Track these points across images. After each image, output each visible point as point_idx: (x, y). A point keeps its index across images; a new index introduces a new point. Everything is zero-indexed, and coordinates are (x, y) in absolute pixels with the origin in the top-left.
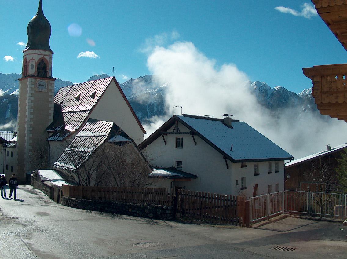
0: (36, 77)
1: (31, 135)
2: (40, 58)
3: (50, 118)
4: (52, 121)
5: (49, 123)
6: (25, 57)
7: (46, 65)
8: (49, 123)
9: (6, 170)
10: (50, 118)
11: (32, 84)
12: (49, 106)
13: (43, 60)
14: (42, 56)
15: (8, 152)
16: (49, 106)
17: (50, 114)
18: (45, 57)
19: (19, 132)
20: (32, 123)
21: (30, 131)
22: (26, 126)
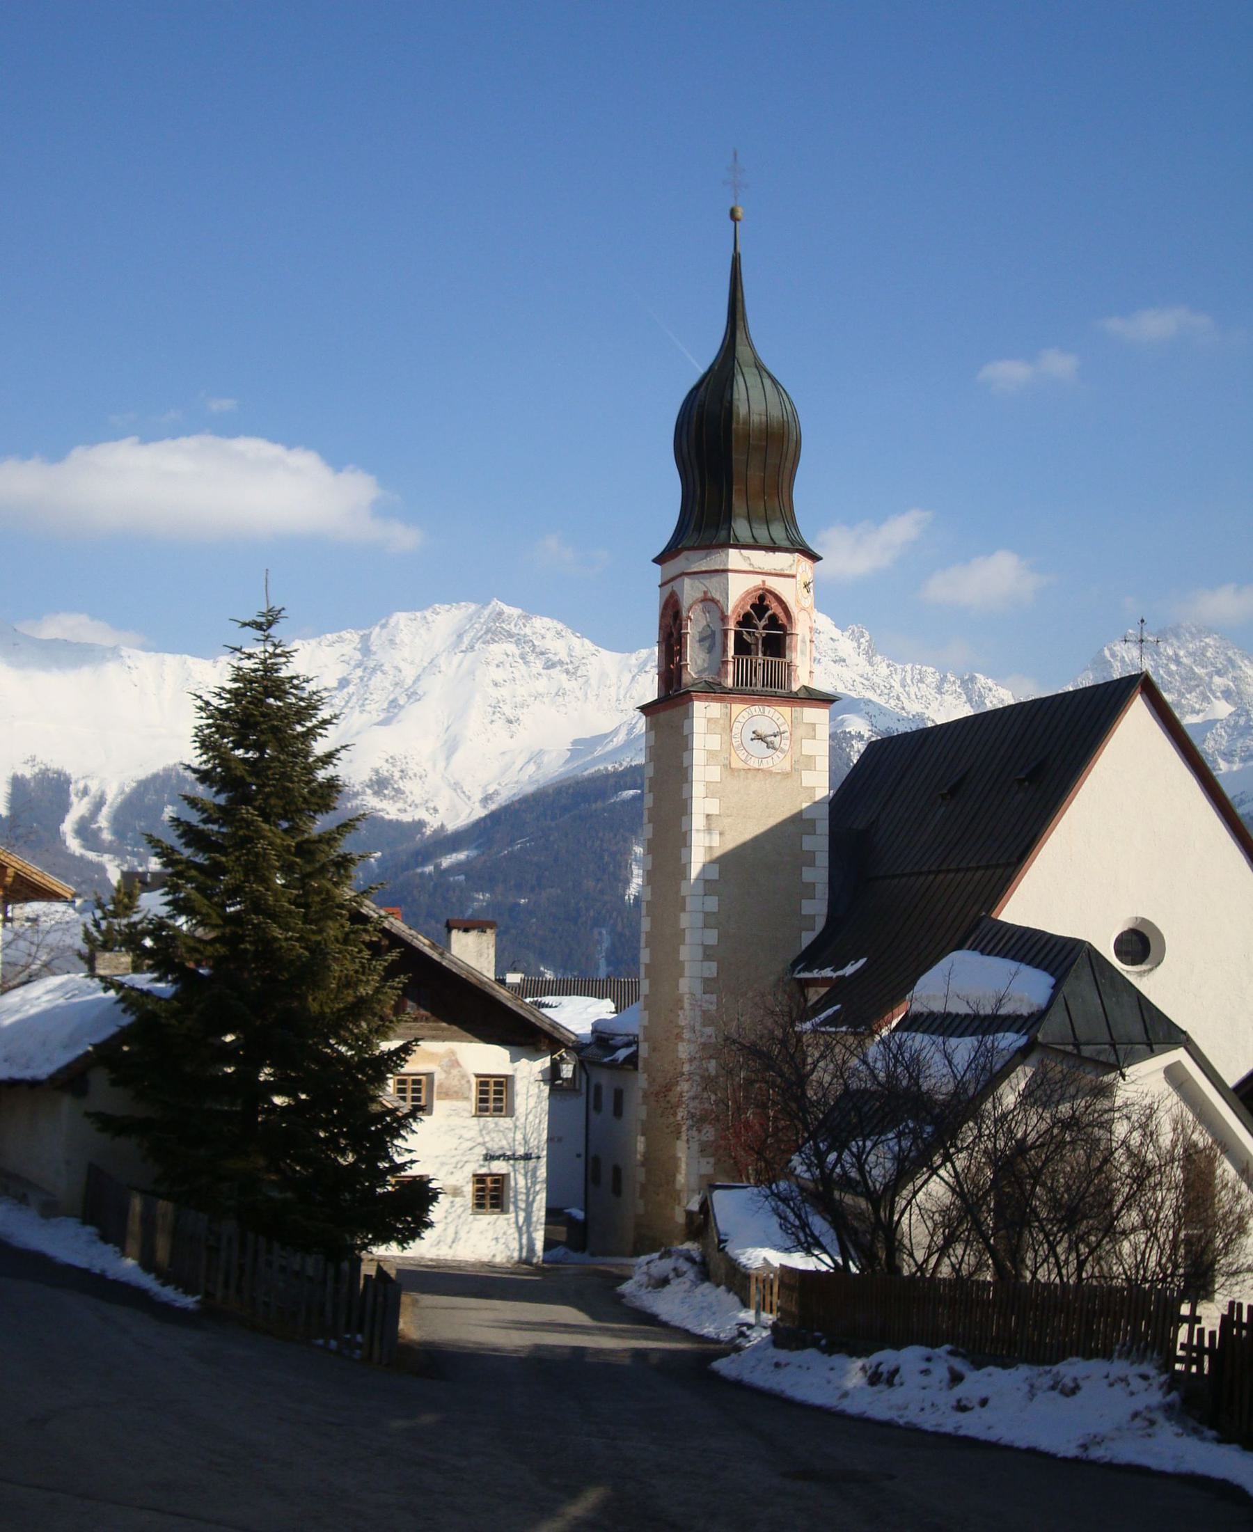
0: (730, 692)
1: (711, 969)
2: (748, 593)
3: (808, 875)
4: (820, 924)
5: (804, 934)
6: (668, 588)
7: (782, 627)
8: (804, 934)
9: (593, 1113)
10: (808, 875)
11: (706, 926)
12: (805, 848)
13: (762, 598)
14: (756, 581)
15: (598, 1088)
16: (805, 848)
17: (808, 891)
18: (774, 584)
19: (656, 770)
20: (712, 937)
21: (706, 981)
22: (686, 1017)
